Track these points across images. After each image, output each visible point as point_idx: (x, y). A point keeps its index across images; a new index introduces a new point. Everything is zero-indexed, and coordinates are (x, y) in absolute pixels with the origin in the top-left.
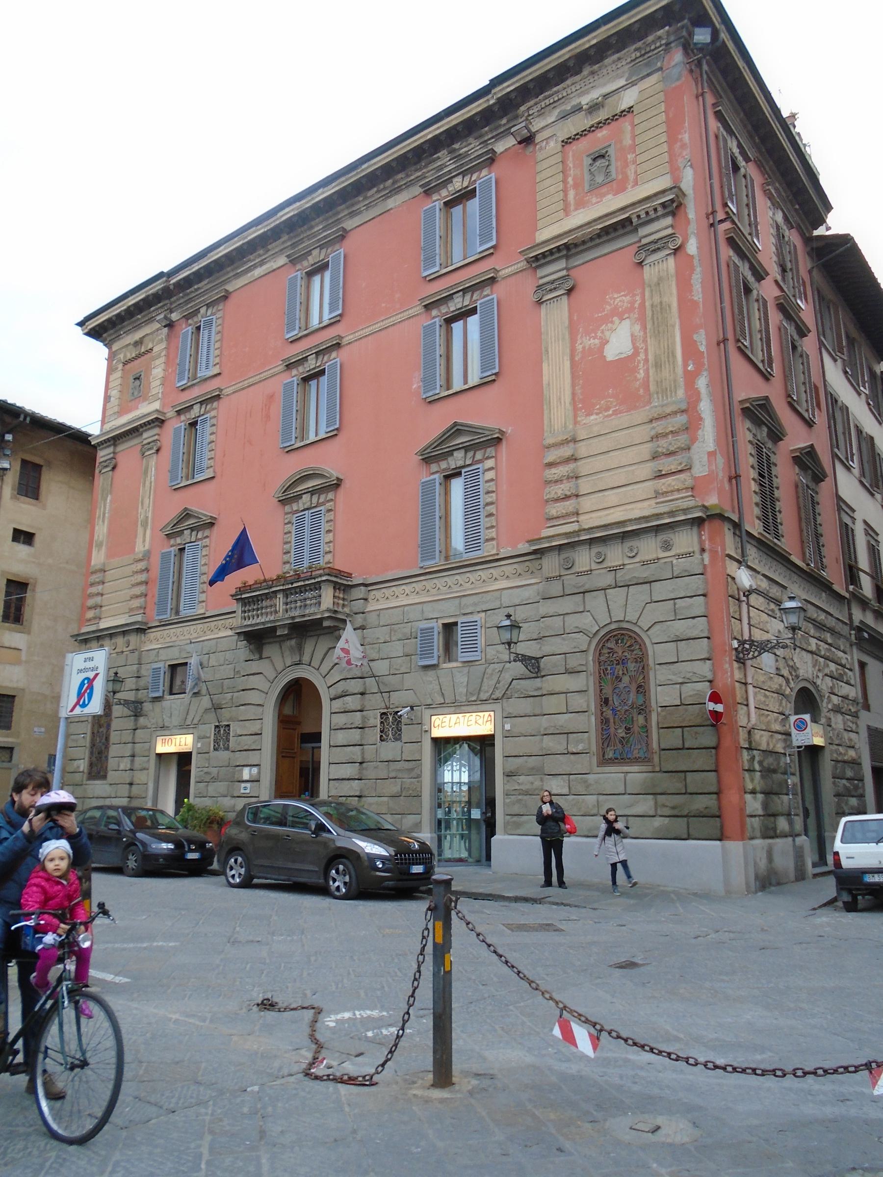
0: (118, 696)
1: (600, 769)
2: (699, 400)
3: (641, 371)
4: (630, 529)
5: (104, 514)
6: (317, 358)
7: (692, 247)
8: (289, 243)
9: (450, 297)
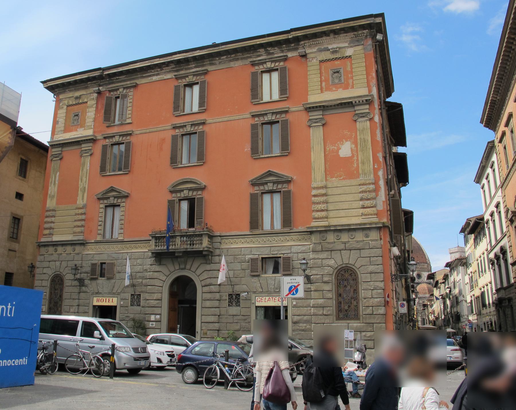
2: (379, 180)
4: (352, 227)
9: (266, 114)
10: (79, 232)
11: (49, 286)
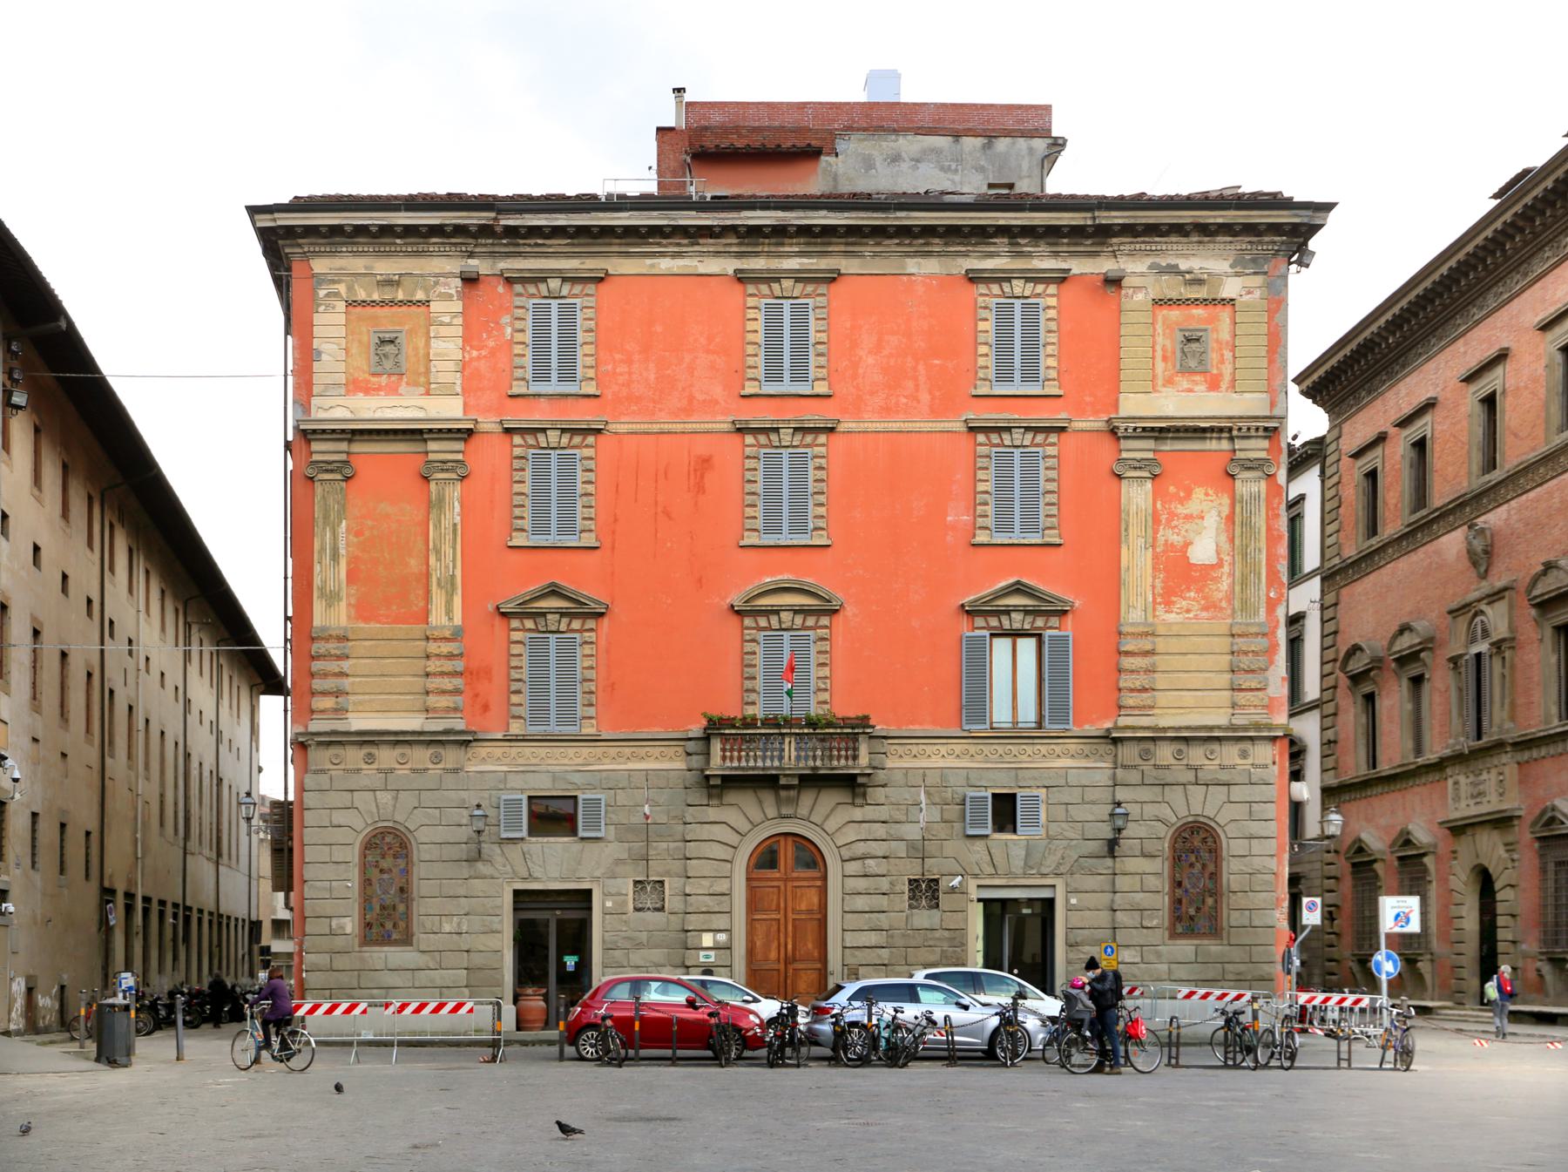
2: (1276, 627)
10: (448, 709)
11: (356, 860)
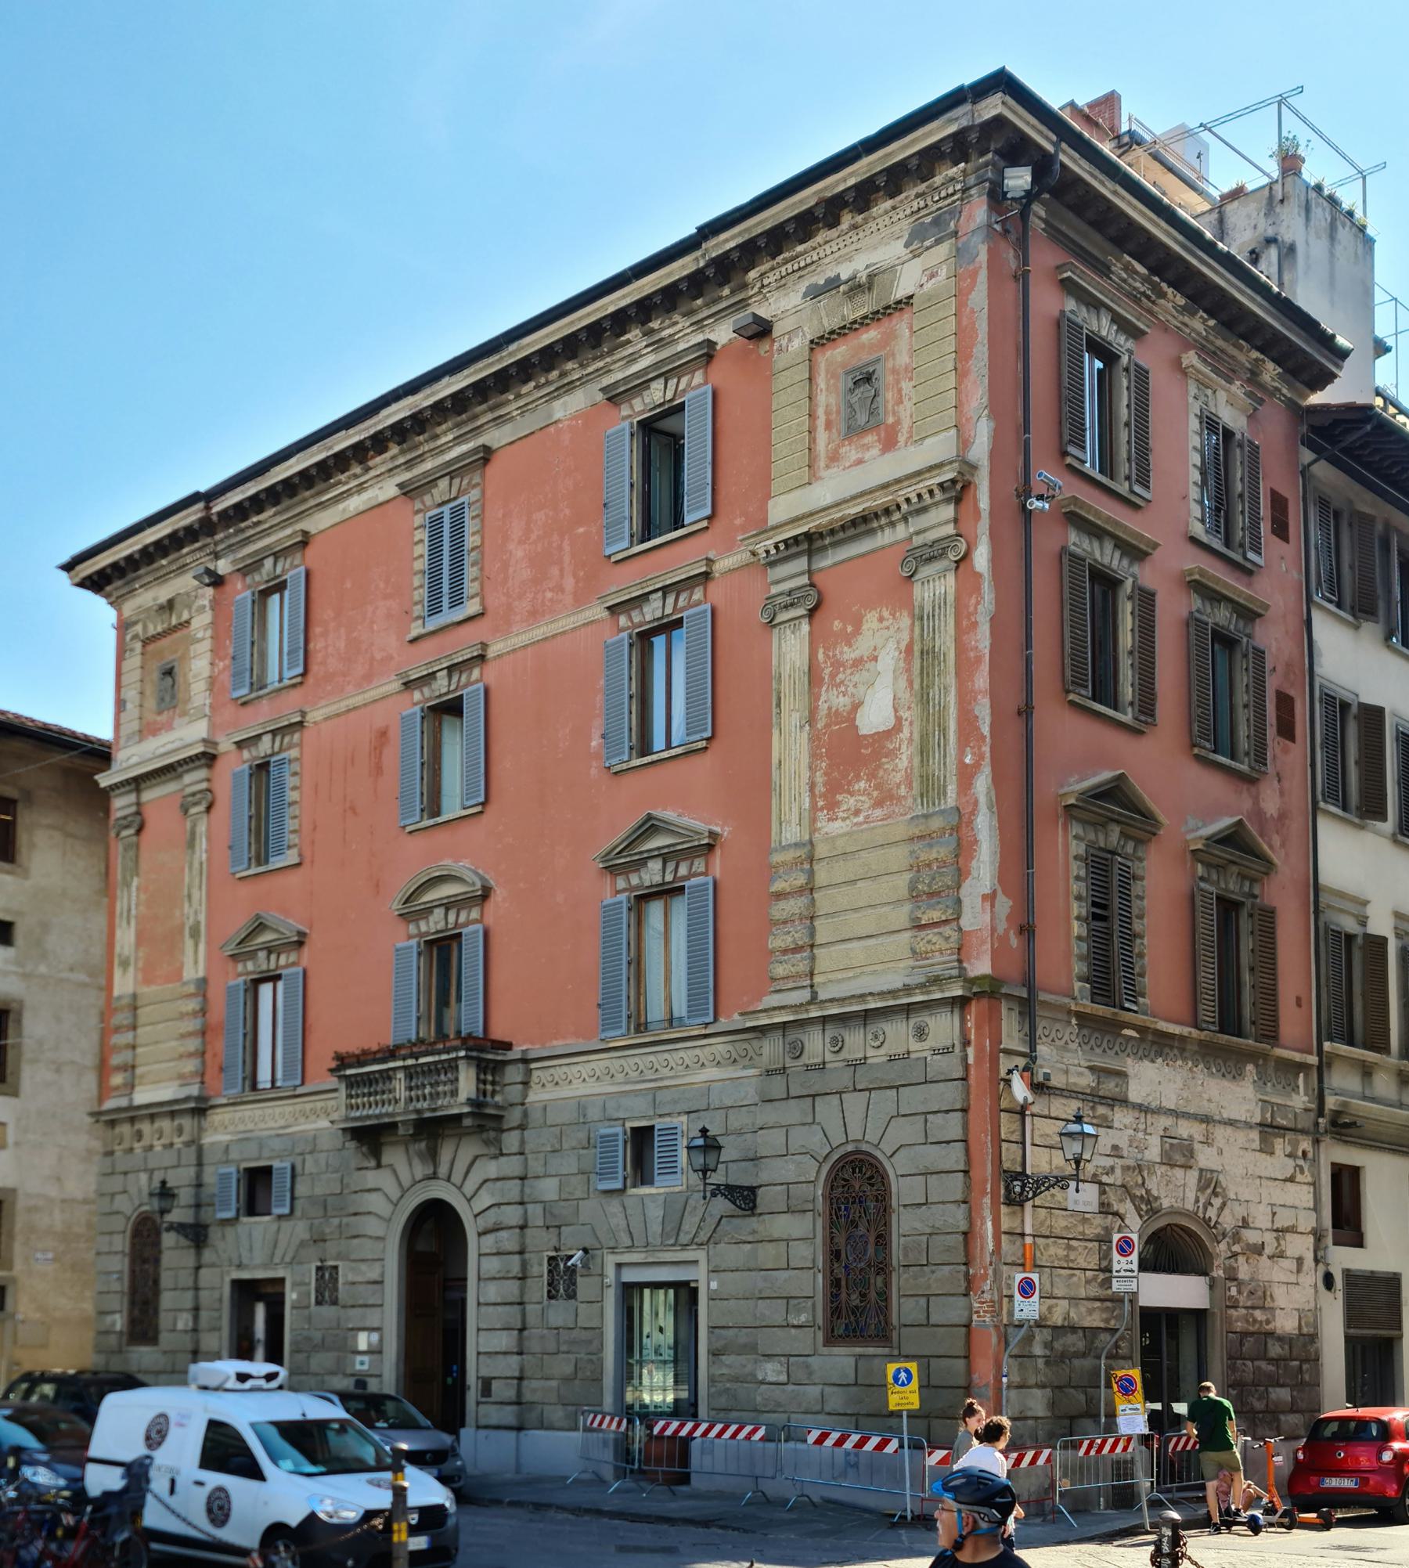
0: (169, 1218)
1: (826, 1351)
2: (974, 813)
3: (904, 757)
5: (129, 910)
6: (450, 676)
7: (981, 559)
8: (401, 460)
9: (645, 597)
